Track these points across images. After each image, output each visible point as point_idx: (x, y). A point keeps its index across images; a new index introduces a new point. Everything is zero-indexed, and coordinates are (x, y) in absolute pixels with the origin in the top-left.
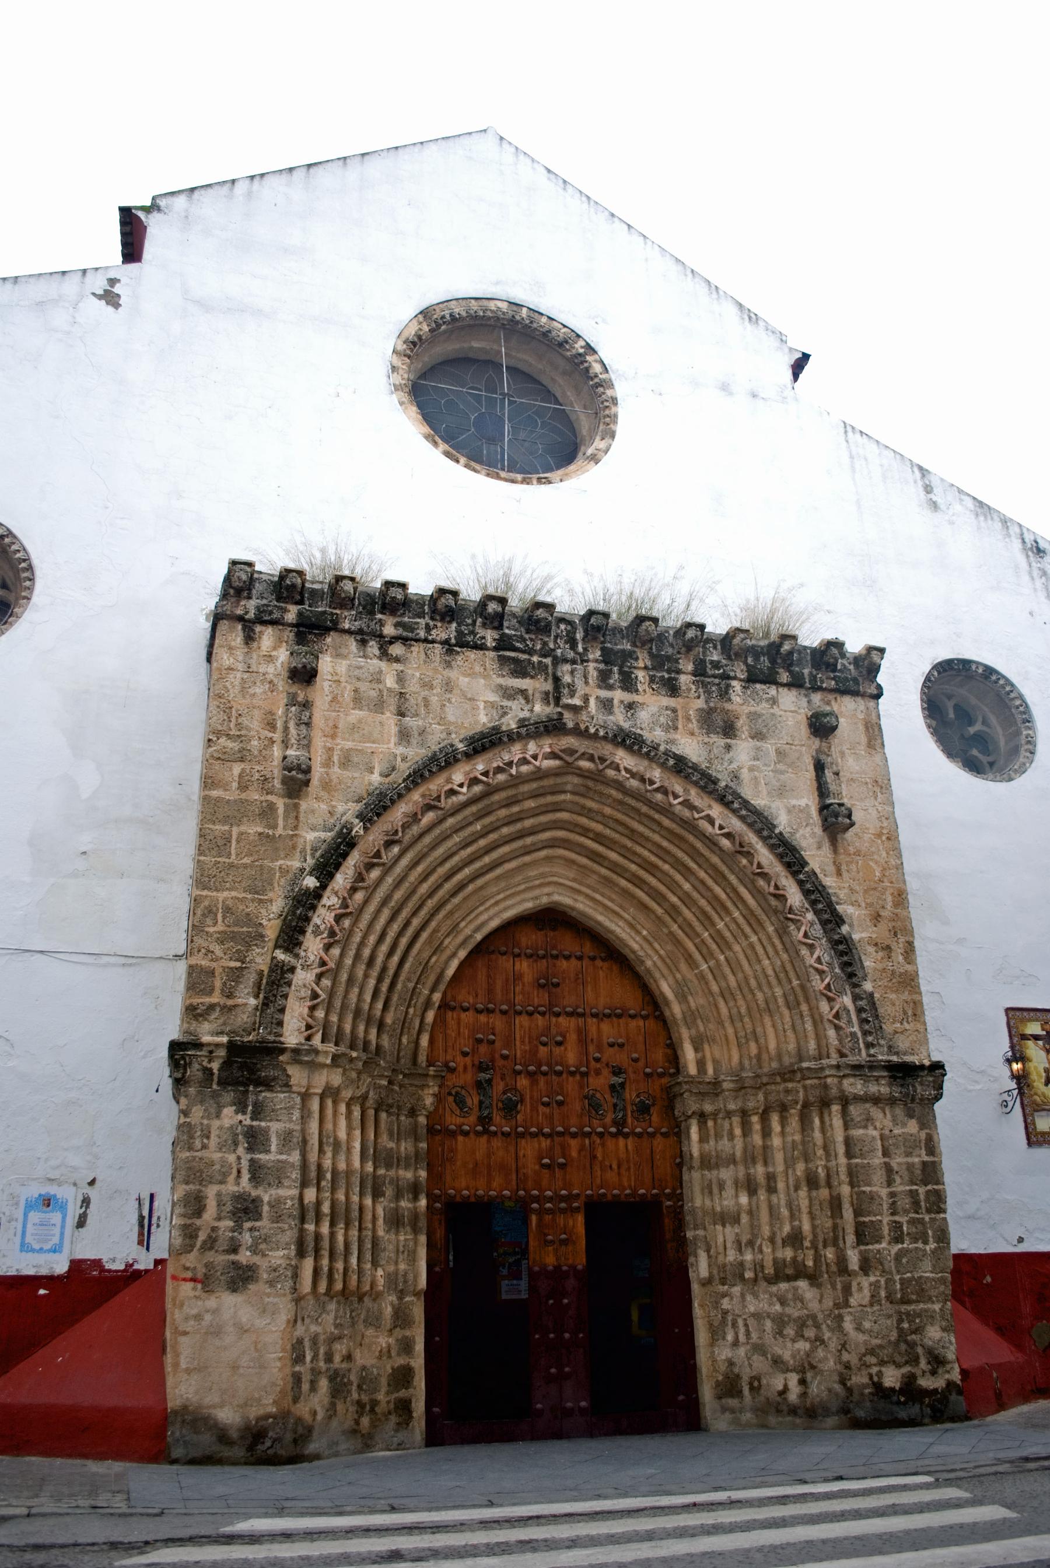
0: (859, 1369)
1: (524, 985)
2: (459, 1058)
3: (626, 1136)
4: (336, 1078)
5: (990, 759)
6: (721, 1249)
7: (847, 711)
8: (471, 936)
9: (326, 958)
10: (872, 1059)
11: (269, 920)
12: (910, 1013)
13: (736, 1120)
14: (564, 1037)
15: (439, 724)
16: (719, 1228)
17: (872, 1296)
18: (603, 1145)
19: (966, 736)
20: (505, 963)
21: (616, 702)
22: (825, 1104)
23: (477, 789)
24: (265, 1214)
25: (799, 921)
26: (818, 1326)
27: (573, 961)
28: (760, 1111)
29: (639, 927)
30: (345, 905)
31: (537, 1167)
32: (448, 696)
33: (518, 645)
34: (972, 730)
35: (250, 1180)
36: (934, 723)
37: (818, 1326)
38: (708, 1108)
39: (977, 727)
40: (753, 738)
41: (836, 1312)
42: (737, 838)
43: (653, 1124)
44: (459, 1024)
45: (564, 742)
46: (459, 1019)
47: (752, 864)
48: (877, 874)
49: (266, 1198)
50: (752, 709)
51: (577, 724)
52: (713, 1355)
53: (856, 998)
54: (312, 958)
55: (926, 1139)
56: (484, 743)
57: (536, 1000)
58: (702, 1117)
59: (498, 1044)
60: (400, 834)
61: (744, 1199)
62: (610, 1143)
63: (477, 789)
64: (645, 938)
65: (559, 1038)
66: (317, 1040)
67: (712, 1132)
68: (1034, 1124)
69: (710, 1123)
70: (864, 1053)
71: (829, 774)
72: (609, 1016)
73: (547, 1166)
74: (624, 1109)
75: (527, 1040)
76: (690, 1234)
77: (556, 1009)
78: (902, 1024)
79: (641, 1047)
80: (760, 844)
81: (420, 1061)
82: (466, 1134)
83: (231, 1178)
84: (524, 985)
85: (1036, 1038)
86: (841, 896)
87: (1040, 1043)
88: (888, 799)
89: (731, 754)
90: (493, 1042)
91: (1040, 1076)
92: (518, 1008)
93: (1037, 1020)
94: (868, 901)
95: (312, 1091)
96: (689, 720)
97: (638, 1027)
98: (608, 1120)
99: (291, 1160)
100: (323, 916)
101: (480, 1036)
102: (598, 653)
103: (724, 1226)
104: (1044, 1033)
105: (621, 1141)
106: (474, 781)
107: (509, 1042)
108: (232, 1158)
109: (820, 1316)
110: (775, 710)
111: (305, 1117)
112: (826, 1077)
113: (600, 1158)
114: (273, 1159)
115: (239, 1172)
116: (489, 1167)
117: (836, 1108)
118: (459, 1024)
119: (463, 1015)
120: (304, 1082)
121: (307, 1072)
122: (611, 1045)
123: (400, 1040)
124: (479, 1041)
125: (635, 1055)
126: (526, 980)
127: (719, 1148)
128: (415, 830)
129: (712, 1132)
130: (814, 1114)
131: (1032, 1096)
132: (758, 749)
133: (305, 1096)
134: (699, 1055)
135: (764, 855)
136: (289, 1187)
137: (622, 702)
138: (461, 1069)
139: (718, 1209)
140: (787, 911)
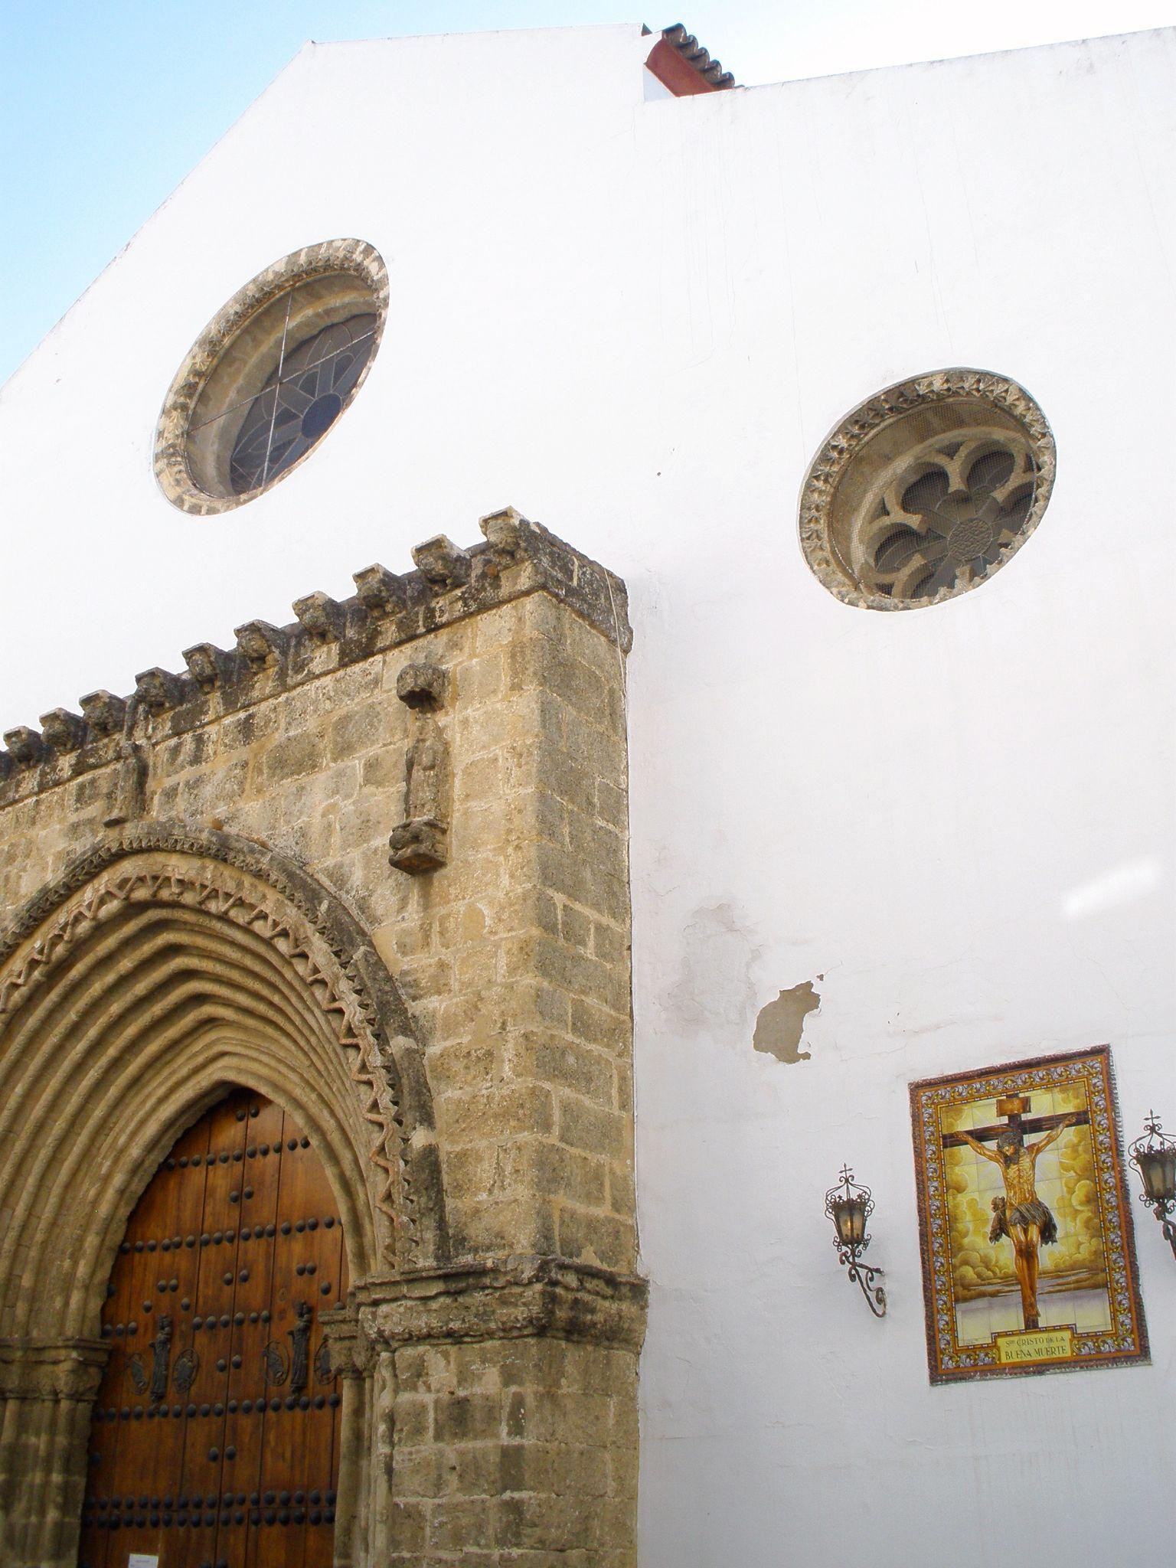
12: (508, 1169)
34: (956, 484)
48: (488, 922)
55: (513, 1405)
68: (953, 1330)
73: (215, 1458)
78: (490, 1191)
82: (139, 1416)
85: (981, 1135)
87: (991, 1145)
91: (979, 1219)
93: (988, 1095)
94: (466, 978)
104: (1005, 1120)
107: (193, 1287)
113: (273, 1443)
124: (163, 1289)
131: (955, 1267)
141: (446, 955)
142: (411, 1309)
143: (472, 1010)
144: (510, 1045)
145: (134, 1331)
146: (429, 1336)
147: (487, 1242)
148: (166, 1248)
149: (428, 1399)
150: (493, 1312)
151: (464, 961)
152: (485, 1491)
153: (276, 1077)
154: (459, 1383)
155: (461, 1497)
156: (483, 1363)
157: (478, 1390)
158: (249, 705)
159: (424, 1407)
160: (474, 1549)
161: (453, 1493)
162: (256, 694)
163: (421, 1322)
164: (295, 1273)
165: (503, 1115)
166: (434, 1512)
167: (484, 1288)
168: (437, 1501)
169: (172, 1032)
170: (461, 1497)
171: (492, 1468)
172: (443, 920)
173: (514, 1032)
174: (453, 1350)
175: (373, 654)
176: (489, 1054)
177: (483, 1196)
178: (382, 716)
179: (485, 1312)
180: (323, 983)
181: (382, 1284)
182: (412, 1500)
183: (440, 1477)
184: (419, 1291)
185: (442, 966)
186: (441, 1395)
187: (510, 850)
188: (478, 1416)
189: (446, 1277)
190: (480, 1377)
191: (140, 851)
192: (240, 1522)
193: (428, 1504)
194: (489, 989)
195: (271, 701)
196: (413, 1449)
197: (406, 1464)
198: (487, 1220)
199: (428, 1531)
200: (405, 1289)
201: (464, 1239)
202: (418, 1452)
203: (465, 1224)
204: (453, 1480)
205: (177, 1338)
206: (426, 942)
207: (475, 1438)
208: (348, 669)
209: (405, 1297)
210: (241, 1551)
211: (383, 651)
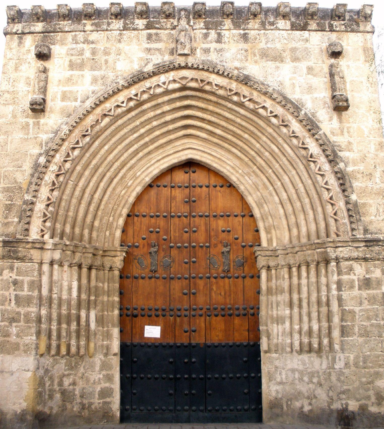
0: (337, 401)
1: (176, 202)
2: (141, 241)
4: (57, 255)
6: (276, 337)
7: (351, 42)
8: (143, 179)
9: (50, 197)
10: (353, 237)
11: (24, 180)
13: (286, 270)
14: (197, 228)
15: (112, 72)
16: (275, 325)
17: (346, 364)
18: (217, 283)
20: (166, 192)
21: (212, 50)
22: (327, 262)
23: (132, 104)
24: (22, 320)
25: (316, 161)
27: (204, 188)
28: (297, 265)
29: (237, 169)
30: (60, 169)
31: (181, 295)
32: (118, 57)
33: (157, 26)
35: (15, 304)
38: (272, 264)
40: (292, 62)
41: (328, 370)
42: (281, 117)
43: (245, 272)
44: (141, 224)
45: (180, 74)
46: (141, 221)
47: (289, 131)
49: (22, 313)
50: (294, 46)
51: (187, 63)
52: (270, 389)
53: (347, 203)
54: (44, 197)
56: (138, 78)
57: (183, 209)
58: (269, 268)
59: (161, 233)
60: (89, 131)
62: (221, 282)
63: (132, 104)
64: (240, 174)
65: (194, 229)
66: (47, 237)
67: (274, 276)
69: (273, 271)
70: (350, 234)
71: (337, 78)
72: (222, 216)
74: (229, 264)
75: (177, 230)
76: (261, 328)
77: (194, 214)
79: (240, 232)
80: (294, 120)
81: (115, 243)
82: (143, 278)
83: (7, 303)
84: (176, 202)
86: (343, 147)
88: (376, 91)
89: (279, 71)
90: (158, 232)
92: (173, 214)
94: (360, 149)
95: (43, 262)
96: (255, 55)
97: (239, 221)
98: (220, 270)
99: (33, 294)
100: (49, 177)
101: (152, 229)
102: (202, 24)
103: (278, 324)
105: (226, 280)
106: (130, 99)
107: (167, 232)
108: (7, 293)
110: (308, 45)
111: (40, 274)
112: (327, 248)
114: (25, 294)
115: (10, 300)
116: (155, 294)
117: (333, 264)
118: (141, 224)
119: (143, 219)
120: (39, 257)
121: (40, 253)
122: (223, 231)
123: (105, 233)
124: (151, 232)
125: (236, 236)
126: (178, 200)
127: (278, 284)
128: (98, 128)
129: (274, 276)
130: (322, 268)
132: (295, 67)
133: (41, 263)
134: (269, 236)
135: (295, 126)
136: (32, 307)
137: (215, 49)
138: (141, 246)
139: (275, 316)
140: (309, 156)
141: (351, 140)
142: (351, 250)
143: (363, 159)
144: (378, 173)
145: (137, 247)
146: (357, 259)
147: (376, 231)
148: (152, 217)
149: (355, 278)
150: (381, 253)
151: (358, 143)
152: (377, 305)
153: (222, 163)
154: (367, 273)
155: (369, 307)
156: (375, 267)
157: (373, 275)
158: (246, 29)
159: (353, 280)
160: (375, 322)
161: (366, 305)
162: (250, 26)
163: (355, 254)
164: (220, 231)
165: (378, 194)
166: (359, 312)
167: (378, 246)
168: (360, 308)
169: (172, 137)
170: (369, 307)
171: (380, 298)
172: (348, 128)
173: (379, 169)
174: (363, 264)
175: (305, 30)
176: (371, 174)
177: (373, 218)
178: (312, 53)
179: (378, 253)
180: (296, 137)
181: (343, 241)
182: (352, 308)
183: (361, 301)
184: (356, 245)
185: (350, 143)
186: (360, 277)
187: (371, 112)
188: (374, 283)
189: (366, 241)
190: (374, 272)
191: (197, 69)
192: (201, 316)
193: (357, 309)
194: (369, 154)
195: (256, 31)
196: (350, 293)
197: (348, 297)
198: (375, 225)
199: (357, 317)
200: (350, 244)
201: (367, 230)
202: (352, 294)
203: (367, 225)
204: (366, 302)
205: (161, 251)
206: (342, 133)
207: (373, 290)
208: (293, 32)
209: (350, 246)
210: (203, 325)
211: (309, 30)
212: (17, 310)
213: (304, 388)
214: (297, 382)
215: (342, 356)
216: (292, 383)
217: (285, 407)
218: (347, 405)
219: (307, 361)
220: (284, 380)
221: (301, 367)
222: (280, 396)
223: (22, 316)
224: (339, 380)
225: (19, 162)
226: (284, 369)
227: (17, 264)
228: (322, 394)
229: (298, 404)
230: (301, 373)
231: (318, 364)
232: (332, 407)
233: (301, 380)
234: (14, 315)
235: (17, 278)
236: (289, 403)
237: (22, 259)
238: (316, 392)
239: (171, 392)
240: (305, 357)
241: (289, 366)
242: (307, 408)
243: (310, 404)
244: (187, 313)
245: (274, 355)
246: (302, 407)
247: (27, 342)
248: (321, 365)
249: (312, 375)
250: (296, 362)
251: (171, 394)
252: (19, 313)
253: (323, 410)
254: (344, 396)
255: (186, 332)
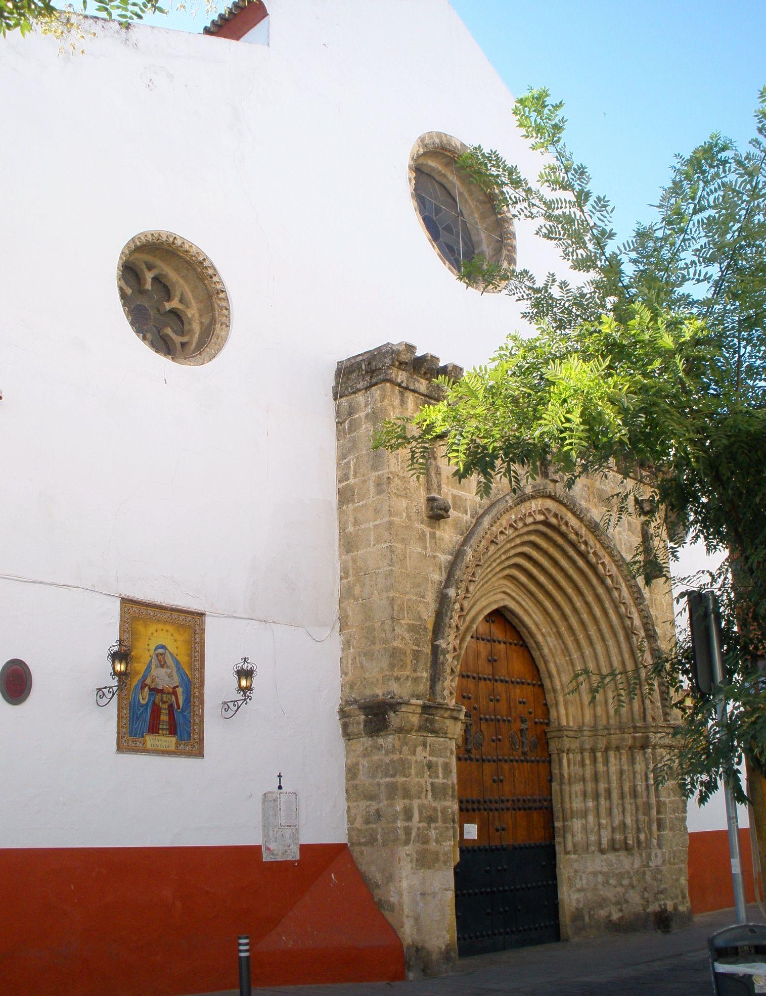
3: (527, 762)
5: (185, 339)
19: (162, 311)
22: (643, 747)
26: (631, 878)
36: (129, 291)
37: (631, 878)
39: (175, 304)
49: (439, 809)
52: (570, 897)
61: (590, 804)
83: (423, 795)
108: (422, 781)
109: (632, 874)
122: (520, 703)
193: (667, 800)
212: (434, 805)
213: (609, 894)
214: (600, 886)
215: (659, 852)
216: (595, 889)
217: (587, 919)
218: (665, 905)
219: (614, 861)
220: (585, 886)
221: (605, 869)
222: (581, 906)
223: (440, 814)
224: (654, 878)
225: (422, 589)
226: (584, 872)
227: (431, 739)
228: (635, 897)
229: (603, 913)
230: (606, 875)
231: (626, 863)
232: (648, 910)
233: (606, 883)
234: (431, 812)
235: (431, 758)
236: (592, 912)
237: (435, 732)
238: (627, 895)
239: (489, 910)
240: (611, 856)
241: (590, 869)
242: (615, 916)
243: (621, 910)
244: (497, 806)
245: (573, 856)
246: (610, 915)
247: (446, 849)
248: (632, 864)
249: (620, 876)
250: (598, 863)
251: (488, 914)
252: (435, 809)
253: (637, 915)
254: (662, 896)
255: (497, 830)
